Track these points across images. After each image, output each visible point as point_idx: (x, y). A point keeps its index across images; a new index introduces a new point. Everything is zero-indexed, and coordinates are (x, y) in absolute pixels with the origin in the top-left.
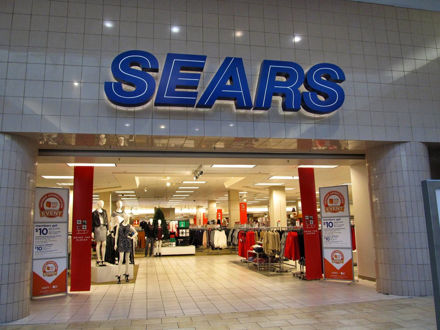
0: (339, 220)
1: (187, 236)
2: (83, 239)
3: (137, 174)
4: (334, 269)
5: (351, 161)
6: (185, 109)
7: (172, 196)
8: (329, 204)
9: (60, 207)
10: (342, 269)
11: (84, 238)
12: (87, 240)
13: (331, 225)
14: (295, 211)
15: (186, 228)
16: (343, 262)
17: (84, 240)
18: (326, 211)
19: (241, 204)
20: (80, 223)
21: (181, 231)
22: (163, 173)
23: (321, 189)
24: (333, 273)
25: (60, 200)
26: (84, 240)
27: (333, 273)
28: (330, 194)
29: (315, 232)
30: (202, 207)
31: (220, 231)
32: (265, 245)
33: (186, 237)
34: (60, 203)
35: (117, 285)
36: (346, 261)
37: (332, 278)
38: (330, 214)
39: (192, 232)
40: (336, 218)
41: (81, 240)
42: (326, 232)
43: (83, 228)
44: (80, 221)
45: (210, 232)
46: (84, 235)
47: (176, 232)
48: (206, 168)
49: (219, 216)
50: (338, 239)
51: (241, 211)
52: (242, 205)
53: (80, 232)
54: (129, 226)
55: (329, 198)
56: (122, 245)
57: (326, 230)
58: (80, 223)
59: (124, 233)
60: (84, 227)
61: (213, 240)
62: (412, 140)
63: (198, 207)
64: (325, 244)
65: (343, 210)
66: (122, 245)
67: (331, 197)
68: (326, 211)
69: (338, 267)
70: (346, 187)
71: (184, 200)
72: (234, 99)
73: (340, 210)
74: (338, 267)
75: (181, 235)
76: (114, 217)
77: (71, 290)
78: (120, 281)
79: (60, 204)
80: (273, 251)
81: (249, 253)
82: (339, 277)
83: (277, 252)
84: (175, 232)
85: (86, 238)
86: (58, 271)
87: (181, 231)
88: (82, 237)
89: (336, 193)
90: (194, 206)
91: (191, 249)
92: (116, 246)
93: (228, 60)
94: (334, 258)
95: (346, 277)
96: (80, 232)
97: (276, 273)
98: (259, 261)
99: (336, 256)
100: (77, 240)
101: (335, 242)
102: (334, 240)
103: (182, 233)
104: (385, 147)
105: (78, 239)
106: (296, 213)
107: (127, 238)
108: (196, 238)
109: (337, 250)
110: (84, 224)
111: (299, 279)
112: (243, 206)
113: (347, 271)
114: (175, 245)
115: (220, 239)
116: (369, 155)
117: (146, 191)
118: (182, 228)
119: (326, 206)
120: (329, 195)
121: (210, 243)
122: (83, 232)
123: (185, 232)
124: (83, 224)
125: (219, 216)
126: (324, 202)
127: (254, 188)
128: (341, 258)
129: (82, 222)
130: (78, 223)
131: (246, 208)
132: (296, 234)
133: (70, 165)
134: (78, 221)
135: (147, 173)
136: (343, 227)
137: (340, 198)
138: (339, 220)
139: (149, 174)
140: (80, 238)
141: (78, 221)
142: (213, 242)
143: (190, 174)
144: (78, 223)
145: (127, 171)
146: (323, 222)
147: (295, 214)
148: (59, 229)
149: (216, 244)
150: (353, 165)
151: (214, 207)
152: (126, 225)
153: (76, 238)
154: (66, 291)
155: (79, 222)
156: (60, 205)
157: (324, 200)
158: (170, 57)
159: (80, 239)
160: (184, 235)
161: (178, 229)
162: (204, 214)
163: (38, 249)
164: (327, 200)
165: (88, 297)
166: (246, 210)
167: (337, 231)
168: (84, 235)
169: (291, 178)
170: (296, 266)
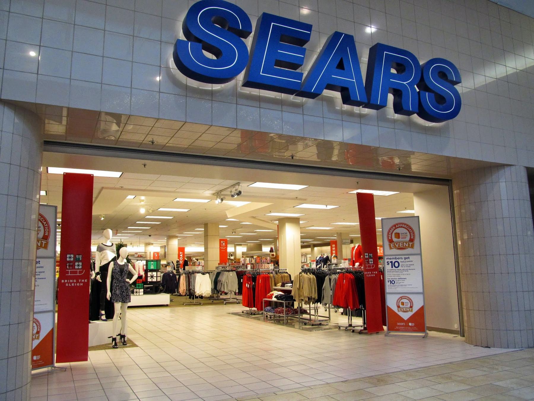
0: (407, 258)
1: (158, 280)
2: (77, 283)
3: (131, 191)
4: (401, 319)
5: (416, 186)
6: (283, 96)
7: (126, 229)
8: (395, 239)
9: (45, 233)
10: (411, 319)
11: (78, 282)
12: (82, 284)
13: (396, 264)
14: (273, 252)
15: (156, 270)
16: (412, 311)
17: (78, 284)
18: (391, 248)
19: (220, 240)
20: (72, 259)
21: (149, 274)
22: (174, 192)
23: (384, 220)
24: (399, 324)
25: (45, 223)
26: (78, 284)
27: (399, 324)
28: (395, 226)
29: (375, 274)
30: (152, 244)
31: (203, 274)
32: (297, 292)
33: (157, 282)
34: (44, 227)
35: (110, 351)
36: (416, 309)
37: (398, 330)
38: (395, 251)
39: (166, 276)
40: (403, 257)
41: (73, 284)
42: (389, 274)
43: (76, 267)
44: (72, 256)
45: (190, 276)
46: (77, 278)
47: (144, 276)
48: (244, 187)
49: (181, 255)
50: (406, 282)
51: (220, 250)
52: (222, 242)
53: (71, 273)
54: (126, 265)
55: (395, 232)
56: (118, 292)
57: (390, 271)
58: (72, 259)
59: (121, 275)
60: (78, 265)
61: (194, 286)
62: (516, 164)
63: (148, 244)
64: (388, 288)
65: (412, 247)
66: (118, 292)
67: (397, 231)
68: (391, 248)
69: (406, 316)
70: (417, 218)
71: (137, 234)
72: (340, 89)
73: (409, 247)
74: (406, 316)
75: (149, 280)
76: (100, 251)
77: (57, 362)
78: (116, 344)
79: (45, 229)
80: (309, 298)
81: (266, 301)
82: (407, 329)
83: (313, 300)
84: (142, 276)
85: (81, 282)
86: (41, 334)
87: (149, 274)
88: (75, 281)
89: (403, 226)
90: (140, 243)
91: (164, 298)
92: (109, 294)
93: (337, 35)
94: (401, 306)
95: (415, 328)
96: (71, 273)
97: (311, 327)
98: (286, 311)
99: (403, 304)
100: (67, 285)
101: (402, 285)
102: (401, 284)
103: (152, 277)
104: (480, 172)
105: (68, 283)
106: (274, 253)
107: (125, 282)
108: (169, 283)
109: (403, 296)
110: (79, 261)
111: (352, 333)
112: (224, 243)
113: (418, 322)
114: (142, 293)
115: (203, 285)
116: (451, 182)
117: (102, 219)
118: (152, 271)
119: (391, 241)
120: (394, 228)
121: (190, 290)
122: (76, 272)
123: (155, 275)
124: (76, 260)
125: (181, 255)
126: (388, 237)
127: (263, 221)
128: (409, 306)
129: (75, 257)
130: (68, 259)
131: (226, 246)
132: (351, 276)
133: (52, 170)
134: (68, 256)
135: (145, 190)
136: (412, 267)
137: (406, 233)
138: (407, 258)
139: (155, 193)
140: (71, 281)
141: (68, 256)
142: (194, 288)
143: (209, 195)
144: (68, 259)
145: (125, 187)
146: (386, 261)
147: (273, 255)
148: (42, 267)
149: (198, 291)
150: (418, 194)
151: (175, 244)
152: (123, 263)
153: (66, 281)
154: (52, 363)
155: (70, 258)
156: (45, 232)
157: (388, 234)
158: (266, 19)
159: (71, 283)
160: (154, 280)
161: (146, 271)
162: (154, 253)
163: (391, 282)
164: (392, 234)
165: (84, 370)
166: (226, 249)
167: (404, 273)
168: (77, 278)
169: (323, 207)
170: (329, 317)
